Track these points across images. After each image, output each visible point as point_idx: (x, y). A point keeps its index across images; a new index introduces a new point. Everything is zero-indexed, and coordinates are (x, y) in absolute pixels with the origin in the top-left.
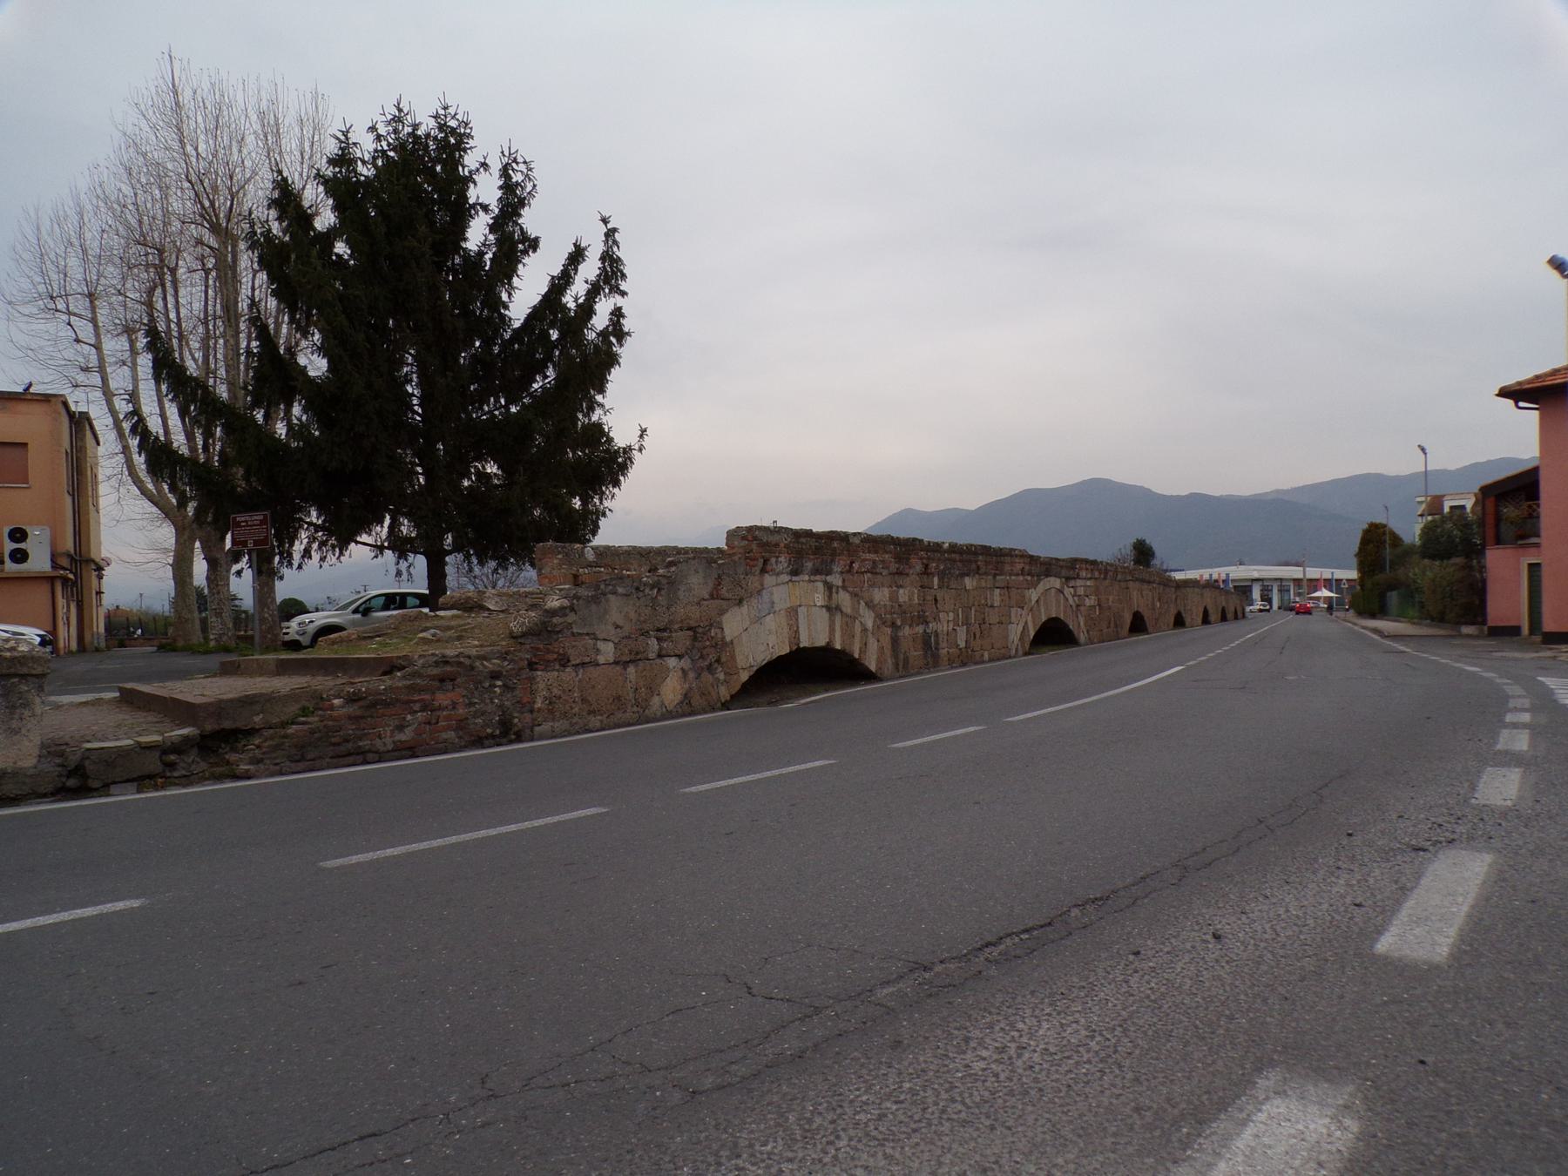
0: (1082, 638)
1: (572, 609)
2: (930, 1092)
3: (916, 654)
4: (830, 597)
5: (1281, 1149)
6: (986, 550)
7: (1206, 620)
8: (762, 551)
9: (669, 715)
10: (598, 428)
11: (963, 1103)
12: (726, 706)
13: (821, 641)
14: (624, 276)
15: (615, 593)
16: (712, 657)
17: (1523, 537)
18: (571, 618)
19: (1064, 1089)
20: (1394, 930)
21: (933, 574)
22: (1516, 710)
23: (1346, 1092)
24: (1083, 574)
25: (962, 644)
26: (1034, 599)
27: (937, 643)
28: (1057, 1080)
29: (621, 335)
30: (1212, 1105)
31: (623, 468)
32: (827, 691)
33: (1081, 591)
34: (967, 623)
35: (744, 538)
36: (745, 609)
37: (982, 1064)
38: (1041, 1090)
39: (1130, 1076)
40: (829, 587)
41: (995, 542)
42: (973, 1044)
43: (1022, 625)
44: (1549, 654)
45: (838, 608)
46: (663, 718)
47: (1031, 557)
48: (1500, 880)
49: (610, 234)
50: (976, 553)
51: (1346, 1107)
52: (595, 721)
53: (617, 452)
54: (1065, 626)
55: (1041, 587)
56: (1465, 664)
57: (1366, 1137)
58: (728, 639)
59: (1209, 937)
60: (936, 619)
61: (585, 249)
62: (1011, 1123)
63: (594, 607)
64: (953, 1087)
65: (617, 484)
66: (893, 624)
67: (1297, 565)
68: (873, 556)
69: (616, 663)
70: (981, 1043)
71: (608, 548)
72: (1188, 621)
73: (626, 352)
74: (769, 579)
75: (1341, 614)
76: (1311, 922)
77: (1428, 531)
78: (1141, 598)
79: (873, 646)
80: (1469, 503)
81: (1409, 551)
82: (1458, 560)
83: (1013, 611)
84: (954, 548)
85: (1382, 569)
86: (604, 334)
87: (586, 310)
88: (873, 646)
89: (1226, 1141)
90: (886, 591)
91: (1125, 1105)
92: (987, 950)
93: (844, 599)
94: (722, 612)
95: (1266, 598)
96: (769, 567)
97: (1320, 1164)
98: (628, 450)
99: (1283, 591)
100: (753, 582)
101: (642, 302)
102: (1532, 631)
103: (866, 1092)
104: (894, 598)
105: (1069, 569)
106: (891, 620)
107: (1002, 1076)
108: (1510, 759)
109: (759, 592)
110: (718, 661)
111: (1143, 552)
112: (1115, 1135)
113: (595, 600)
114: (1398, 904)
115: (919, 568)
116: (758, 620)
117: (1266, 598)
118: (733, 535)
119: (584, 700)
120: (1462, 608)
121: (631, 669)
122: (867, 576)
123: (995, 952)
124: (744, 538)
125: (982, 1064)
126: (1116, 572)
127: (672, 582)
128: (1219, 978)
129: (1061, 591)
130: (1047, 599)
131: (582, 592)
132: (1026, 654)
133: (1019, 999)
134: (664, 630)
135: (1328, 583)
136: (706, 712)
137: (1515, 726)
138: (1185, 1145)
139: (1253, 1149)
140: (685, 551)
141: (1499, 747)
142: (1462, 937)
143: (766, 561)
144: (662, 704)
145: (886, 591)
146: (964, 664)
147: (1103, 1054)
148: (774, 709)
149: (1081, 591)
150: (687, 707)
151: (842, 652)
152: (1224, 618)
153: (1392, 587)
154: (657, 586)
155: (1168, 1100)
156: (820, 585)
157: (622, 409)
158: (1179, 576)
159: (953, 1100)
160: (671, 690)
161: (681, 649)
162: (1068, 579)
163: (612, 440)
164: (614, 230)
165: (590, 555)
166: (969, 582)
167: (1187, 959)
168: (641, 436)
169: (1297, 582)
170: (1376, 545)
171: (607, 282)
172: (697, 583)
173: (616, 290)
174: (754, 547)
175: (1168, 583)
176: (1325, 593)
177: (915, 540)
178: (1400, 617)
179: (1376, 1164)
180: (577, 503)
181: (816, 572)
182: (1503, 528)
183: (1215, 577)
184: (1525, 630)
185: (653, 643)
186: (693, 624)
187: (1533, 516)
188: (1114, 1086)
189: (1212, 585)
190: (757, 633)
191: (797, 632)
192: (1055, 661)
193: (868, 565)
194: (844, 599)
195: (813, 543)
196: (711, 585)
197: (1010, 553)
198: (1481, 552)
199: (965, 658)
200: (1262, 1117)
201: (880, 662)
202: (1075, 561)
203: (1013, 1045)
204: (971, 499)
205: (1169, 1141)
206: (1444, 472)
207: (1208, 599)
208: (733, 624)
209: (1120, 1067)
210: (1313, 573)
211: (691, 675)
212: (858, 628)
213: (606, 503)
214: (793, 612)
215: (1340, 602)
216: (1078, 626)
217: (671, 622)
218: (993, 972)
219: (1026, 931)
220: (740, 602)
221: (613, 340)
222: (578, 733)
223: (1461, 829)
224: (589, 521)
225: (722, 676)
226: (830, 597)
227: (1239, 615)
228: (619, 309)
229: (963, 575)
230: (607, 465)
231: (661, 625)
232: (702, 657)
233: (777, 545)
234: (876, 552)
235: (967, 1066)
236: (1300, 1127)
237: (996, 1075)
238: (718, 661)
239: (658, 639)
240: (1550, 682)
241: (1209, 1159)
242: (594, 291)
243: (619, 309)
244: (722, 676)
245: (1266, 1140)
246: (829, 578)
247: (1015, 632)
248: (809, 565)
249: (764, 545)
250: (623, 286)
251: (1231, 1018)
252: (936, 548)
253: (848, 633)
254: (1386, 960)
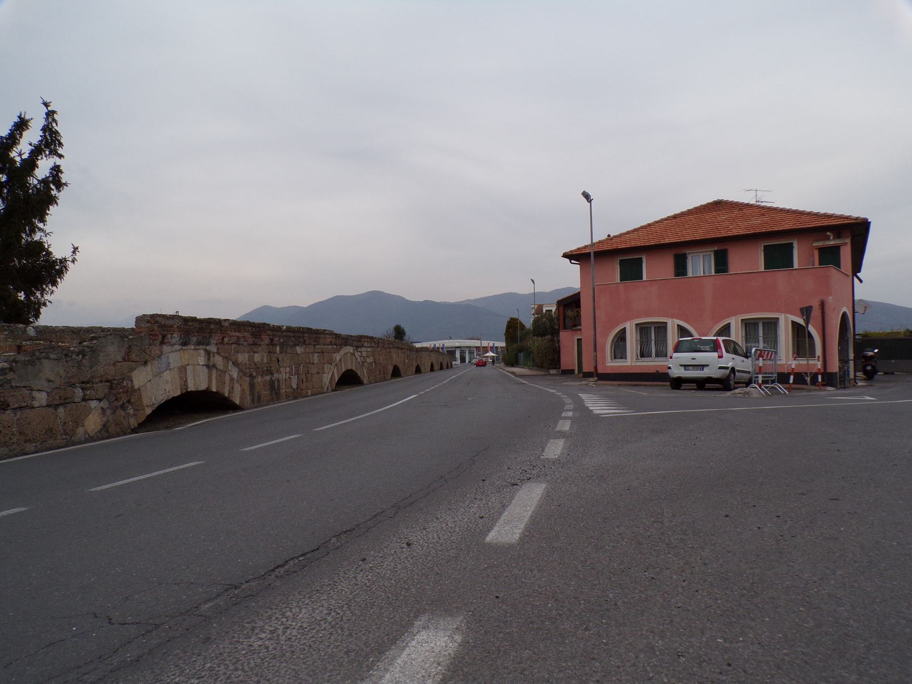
0: (365, 381)
1: (11, 369)
2: (222, 667)
3: (265, 393)
4: (209, 359)
5: (420, 660)
6: (309, 331)
7: (432, 370)
8: (159, 330)
9: (91, 439)
10: (40, 245)
11: (243, 670)
12: (134, 431)
13: (203, 387)
14: (61, 144)
15: (47, 358)
16: (124, 399)
17: (575, 326)
18: (10, 376)
19: (307, 648)
20: (496, 528)
21: (276, 345)
22: (567, 410)
23: (458, 620)
24: (366, 344)
25: (295, 386)
26: (338, 359)
27: (279, 386)
28: (304, 644)
29: (59, 185)
30: (393, 637)
31: (60, 273)
32: (207, 418)
33: (364, 354)
34: (297, 373)
35: (148, 322)
36: (149, 367)
37: (260, 643)
38: (293, 652)
39: (347, 633)
40: (208, 353)
41: (314, 327)
42: (256, 631)
43: (330, 375)
44: (585, 382)
45: (214, 366)
46: (87, 441)
47: (336, 335)
48: (547, 496)
49: (50, 114)
50: (303, 333)
51: (457, 629)
52: (30, 447)
53: (55, 262)
54: (356, 374)
55: (342, 352)
56: (552, 389)
57: (464, 644)
58: (136, 387)
59: (404, 545)
60: (278, 371)
61: (28, 121)
62: (270, 676)
63: (30, 368)
64: (238, 660)
65: (54, 283)
66: (251, 375)
67: (478, 339)
68: (237, 334)
69: (48, 406)
70: (262, 630)
71: (46, 327)
72: (422, 370)
73: (62, 196)
74: (166, 348)
75: (497, 365)
76: (457, 529)
77: (536, 322)
78: (397, 358)
79: (237, 389)
80: (554, 309)
81: (528, 332)
82: (549, 337)
83: (326, 366)
84: (289, 329)
85: (517, 342)
86: (45, 181)
87: (30, 164)
88: (237, 389)
89: (394, 659)
90: (246, 355)
91: (340, 651)
92: (277, 570)
93: (218, 360)
94: (132, 370)
95: (463, 360)
96: (166, 341)
97: (438, 664)
98: (63, 261)
99: (471, 353)
100: (155, 350)
101: (73, 160)
102: (579, 372)
103: (179, 676)
104: (251, 359)
105: (357, 341)
106: (249, 373)
107: (271, 648)
108: (562, 435)
109: (159, 357)
110: (129, 402)
111: (399, 332)
112: (331, 671)
113: (31, 363)
114: (501, 514)
115: (267, 341)
116: (159, 374)
117: (463, 360)
118: (140, 320)
119: (21, 433)
120: (550, 361)
121: (61, 410)
122: (233, 346)
123: (282, 570)
124: (148, 322)
125: (260, 643)
126: (384, 343)
127: (94, 351)
128: (406, 568)
129: (353, 354)
130: (345, 358)
131: (21, 357)
132: (333, 391)
133: (291, 598)
134: (88, 382)
135: (493, 349)
136: (120, 436)
137: (565, 418)
138: (369, 668)
139: (405, 663)
140: (108, 330)
141: (557, 429)
142: (526, 529)
143: (164, 337)
144: (86, 432)
145: (246, 355)
146: (296, 398)
147: (333, 623)
148: (169, 431)
149: (364, 354)
150: (105, 432)
151: (217, 393)
152: (441, 368)
153: (521, 351)
154: (82, 353)
155: (365, 643)
156: (202, 352)
157: (58, 232)
158: (418, 345)
159: (237, 669)
160: (93, 422)
161: (101, 394)
162: (357, 347)
163: (50, 253)
164: (54, 112)
165: (31, 331)
166: (299, 349)
167: (391, 558)
168: (74, 252)
169: (478, 348)
170: (513, 328)
171: (47, 145)
172: (113, 351)
173: (54, 153)
174: (155, 327)
175: (412, 349)
176: (490, 354)
177: (265, 324)
178: (524, 366)
179: (466, 657)
180: (22, 296)
181: (199, 343)
182: (567, 321)
183: (437, 345)
184: (576, 372)
185: (79, 392)
186: (110, 378)
187: (578, 315)
188: (336, 641)
189: (435, 350)
190: (156, 384)
191: (186, 381)
192: (351, 394)
193: (234, 339)
194: (218, 360)
195: (197, 325)
196: (123, 353)
197: (323, 332)
198: (558, 334)
199: (296, 394)
200: (414, 643)
201: (242, 398)
202: (361, 337)
203: (281, 628)
204: (305, 302)
205: (361, 667)
206: (544, 293)
207: (433, 357)
208: (140, 377)
209: (342, 629)
210: (485, 343)
211: (109, 412)
212: (227, 378)
213: (46, 297)
214: (183, 369)
215: (498, 358)
216: (363, 374)
217: (93, 377)
218: (278, 583)
219: (303, 555)
220: (145, 363)
221: (52, 186)
222: (16, 456)
223: (535, 472)
224: (35, 308)
225: (131, 412)
226: (209, 359)
227: (449, 366)
228: (58, 166)
229: (295, 345)
230: (49, 271)
231: (85, 379)
232: (116, 400)
233: (171, 326)
234: (239, 331)
235: (251, 645)
236: (432, 645)
237: (267, 648)
238: (129, 402)
239: (83, 389)
240: (583, 396)
241: (382, 674)
242: (37, 151)
243: (58, 166)
244: (131, 412)
245: (413, 656)
246: (208, 348)
247: (326, 378)
248: (195, 339)
249: (162, 326)
250: (60, 151)
251: (408, 589)
252: (278, 329)
253: (221, 382)
254: (490, 546)
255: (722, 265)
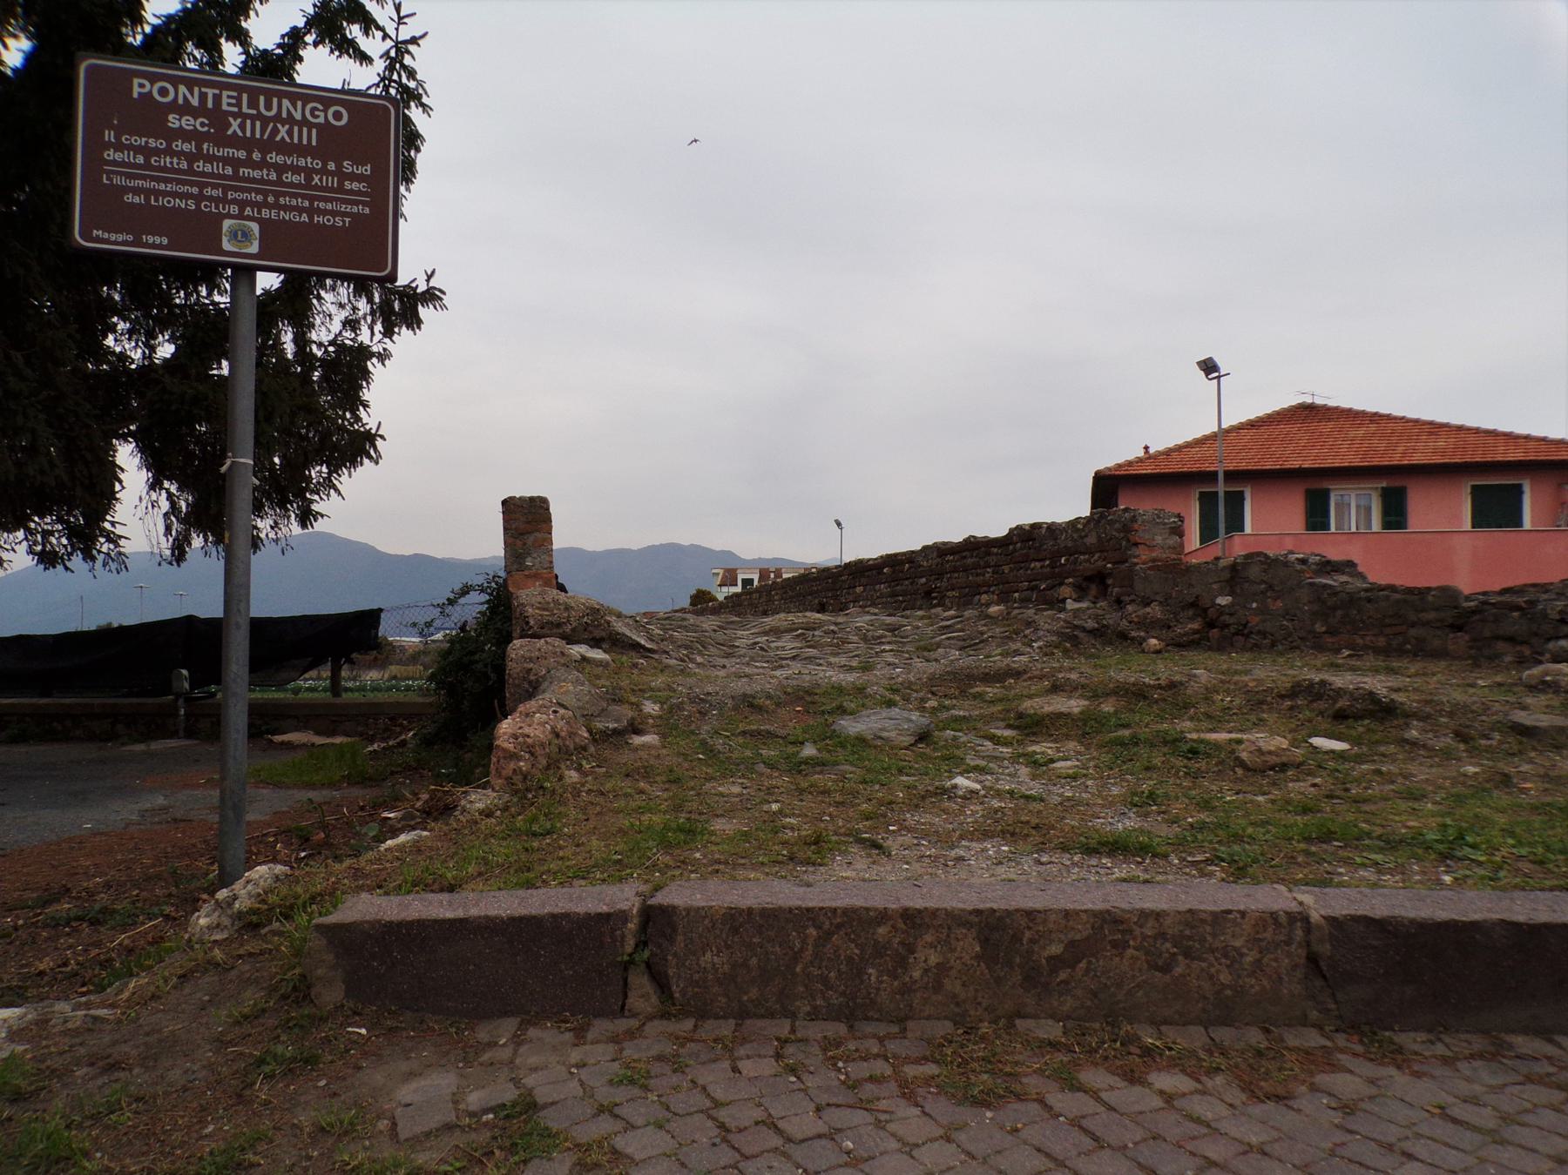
255: (1395, 515)
